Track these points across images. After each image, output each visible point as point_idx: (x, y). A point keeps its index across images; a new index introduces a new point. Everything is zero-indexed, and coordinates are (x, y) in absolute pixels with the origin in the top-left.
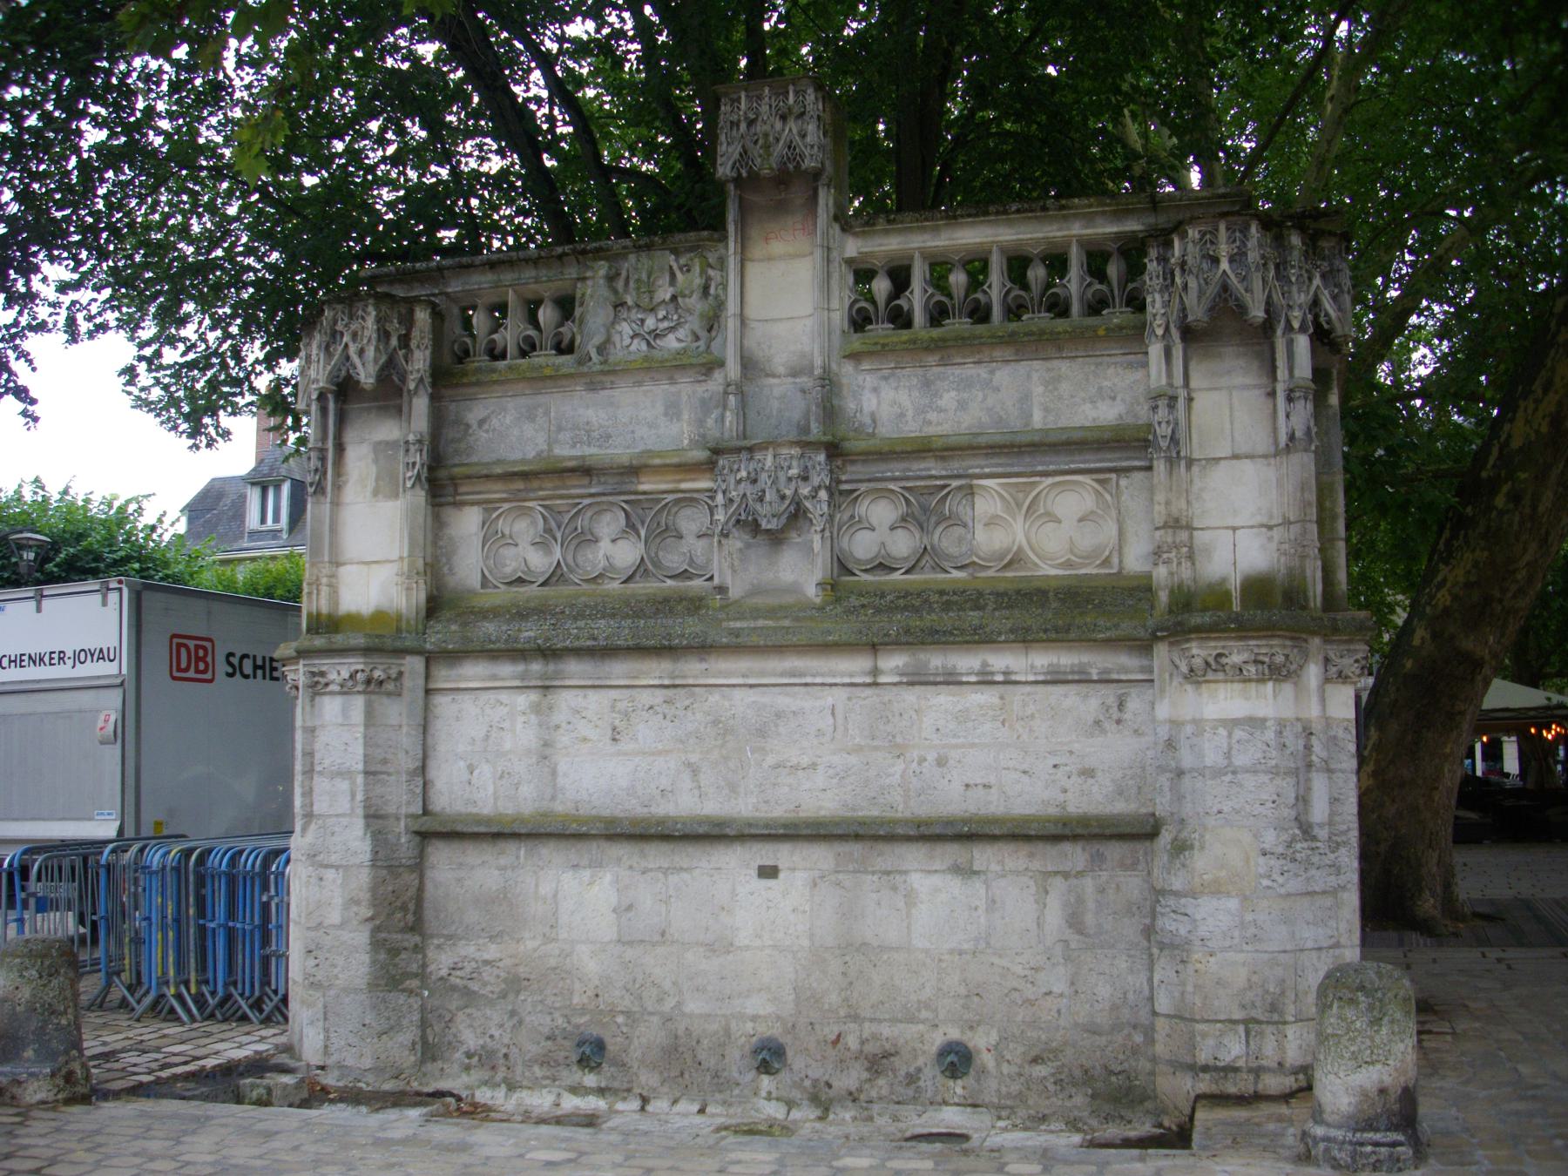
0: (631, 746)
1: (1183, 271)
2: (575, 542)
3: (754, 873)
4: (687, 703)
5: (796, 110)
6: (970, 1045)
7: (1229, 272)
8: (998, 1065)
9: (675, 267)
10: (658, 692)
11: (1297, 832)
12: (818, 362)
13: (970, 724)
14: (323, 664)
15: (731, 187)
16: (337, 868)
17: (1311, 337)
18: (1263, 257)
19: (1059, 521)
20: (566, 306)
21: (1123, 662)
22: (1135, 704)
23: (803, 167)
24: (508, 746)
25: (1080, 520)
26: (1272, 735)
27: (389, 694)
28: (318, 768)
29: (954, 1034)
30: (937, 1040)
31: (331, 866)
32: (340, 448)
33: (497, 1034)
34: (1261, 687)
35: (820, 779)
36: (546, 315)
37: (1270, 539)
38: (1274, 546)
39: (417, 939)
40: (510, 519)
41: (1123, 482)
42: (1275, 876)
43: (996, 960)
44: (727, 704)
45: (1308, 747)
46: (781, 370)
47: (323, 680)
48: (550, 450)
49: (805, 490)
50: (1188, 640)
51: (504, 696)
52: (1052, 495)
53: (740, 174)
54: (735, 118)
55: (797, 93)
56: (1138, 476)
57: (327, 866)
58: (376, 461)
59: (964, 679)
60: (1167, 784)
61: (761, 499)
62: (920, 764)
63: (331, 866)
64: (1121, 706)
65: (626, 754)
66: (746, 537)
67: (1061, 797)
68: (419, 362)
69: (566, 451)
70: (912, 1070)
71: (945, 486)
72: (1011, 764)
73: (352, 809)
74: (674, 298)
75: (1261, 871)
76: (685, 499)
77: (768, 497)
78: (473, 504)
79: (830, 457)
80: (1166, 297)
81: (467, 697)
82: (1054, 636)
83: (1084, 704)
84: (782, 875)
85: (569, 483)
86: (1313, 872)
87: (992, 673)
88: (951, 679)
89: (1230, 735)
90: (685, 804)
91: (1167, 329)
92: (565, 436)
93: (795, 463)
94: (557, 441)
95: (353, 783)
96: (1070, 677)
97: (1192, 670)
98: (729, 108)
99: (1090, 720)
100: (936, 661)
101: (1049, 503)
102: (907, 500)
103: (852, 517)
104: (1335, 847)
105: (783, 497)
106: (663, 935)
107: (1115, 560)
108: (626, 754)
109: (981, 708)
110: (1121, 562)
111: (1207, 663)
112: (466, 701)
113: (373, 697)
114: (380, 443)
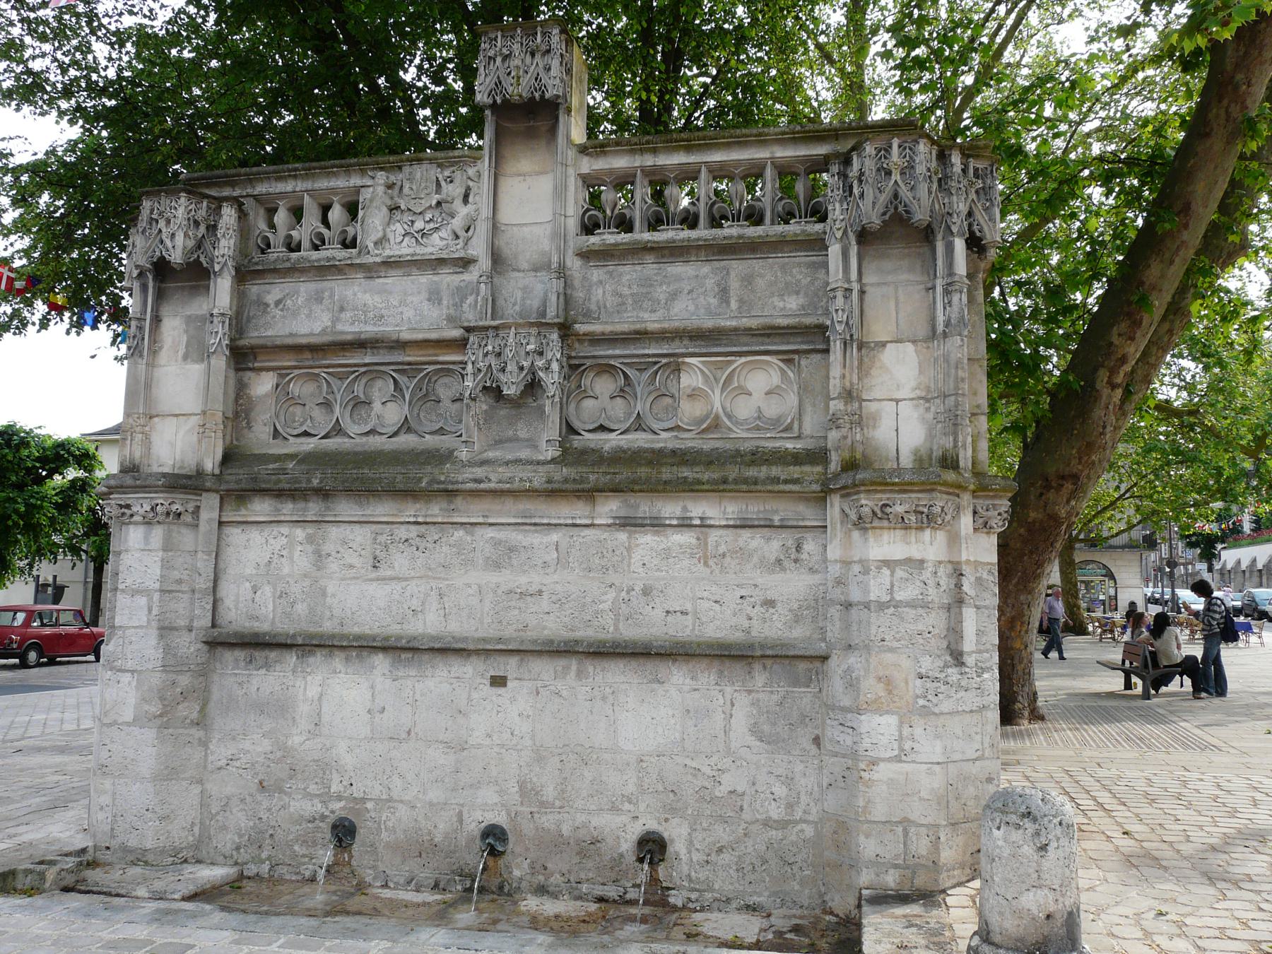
0: (389, 573)
1: (860, 181)
2: (352, 403)
3: (488, 682)
4: (436, 537)
5: (544, 48)
6: (666, 835)
7: (900, 182)
8: (689, 852)
9: (441, 178)
10: (413, 527)
11: (949, 658)
12: (555, 259)
13: (671, 560)
14: (130, 498)
15: (488, 112)
16: (133, 672)
17: (966, 241)
18: (929, 170)
19: (750, 394)
20: (352, 209)
21: (807, 514)
22: (810, 546)
23: (547, 96)
24: (286, 570)
25: (767, 393)
26: (929, 575)
27: (187, 525)
28: (121, 586)
29: (653, 825)
30: (635, 831)
31: (128, 671)
32: (157, 320)
33: (264, 817)
34: (920, 534)
35: (545, 604)
36: (336, 214)
37: (928, 409)
38: (930, 416)
39: (202, 733)
40: (299, 383)
41: (803, 362)
42: (930, 697)
43: (688, 762)
44: (469, 538)
45: (959, 586)
46: (525, 266)
47: (128, 512)
48: (334, 326)
49: (540, 363)
50: (858, 493)
51: (285, 529)
52: (744, 372)
53: (495, 101)
54: (491, 53)
55: (544, 34)
56: (816, 358)
57: (121, 670)
58: (186, 331)
59: (667, 522)
60: (837, 615)
61: (503, 370)
62: (628, 592)
63: (128, 671)
64: (799, 548)
65: (384, 579)
66: (491, 401)
67: (746, 624)
68: (226, 246)
69: (349, 328)
70: (615, 855)
71: (656, 363)
72: (705, 594)
73: (149, 621)
74: (439, 204)
75: (919, 692)
76: (442, 369)
77: (509, 368)
78: (268, 369)
79: (563, 337)
80: (845, 206)
81: (254, 528)
82: (155, 611)
83: (771, 546)
84: (509, 684)
85: (408, 352)
86: (962, 693)
87: (691, 518)
88: (655, 522)
89: (892, 575)
90: (429, 624)
91: (845, 232)
92: (347, 315)
93: (532, 339)
94: (338, 319)
95: (150, 599)
96: (756, 523)
97: (860, 518)
98: (487, 46)
99: (773, 559)
100: (645, 507)
101: (742, 378)
102: (624, 373)
103: (580, 386)
104: (981, 671)
105: (522, 368)
106: (409, 733)
107: (796, 426)
108: (384, 579)
109: (681, 546)
110: (800, 428)
111: (874, 513)
112: (255, 535)
113: (172, 527)
114: (189, 317)
